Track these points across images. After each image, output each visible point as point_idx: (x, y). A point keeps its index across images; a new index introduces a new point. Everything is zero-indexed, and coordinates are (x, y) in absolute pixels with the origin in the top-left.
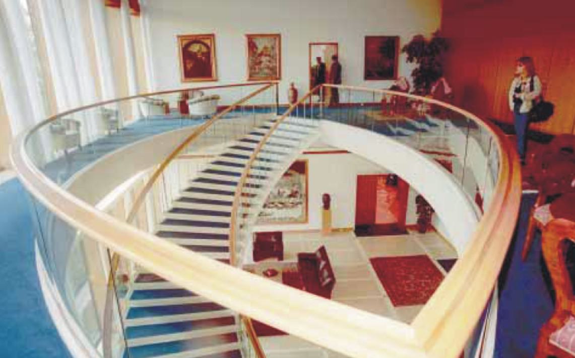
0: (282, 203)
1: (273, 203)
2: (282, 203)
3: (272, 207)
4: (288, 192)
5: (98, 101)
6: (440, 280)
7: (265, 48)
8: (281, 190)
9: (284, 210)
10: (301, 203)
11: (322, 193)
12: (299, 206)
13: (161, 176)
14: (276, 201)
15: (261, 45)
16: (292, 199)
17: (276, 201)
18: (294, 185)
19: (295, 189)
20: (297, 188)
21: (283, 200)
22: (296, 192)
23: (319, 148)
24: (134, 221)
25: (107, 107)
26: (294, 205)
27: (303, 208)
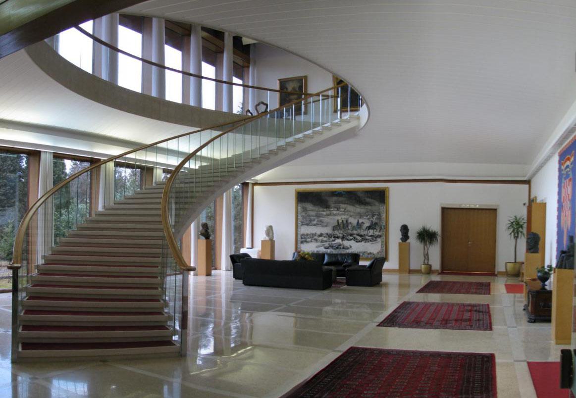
0: (361, 236)
1: (351, 235)
2: (361, 236)
3: (351, 240)
4: (367, 224)
5: (246, 88)
6: (382, 208)
7: (294, 88)
8: (360, 221)
9: (363, 243)
10: (380, 236)
11: (402, 224)
12: (379, 240)
13: (212, 142)
14: (355, 232)
15: (290, 87)
16: (371, 232)
17: (355, 232)
18: (373, 216)
19: (374, 220)
20: (377, 218)
21: (362, 233)
22: (376, 224)
23: (466, 176)
24: (338, 80)
25: (240, 82)
26: (374, 238)
27: (382, 242)
